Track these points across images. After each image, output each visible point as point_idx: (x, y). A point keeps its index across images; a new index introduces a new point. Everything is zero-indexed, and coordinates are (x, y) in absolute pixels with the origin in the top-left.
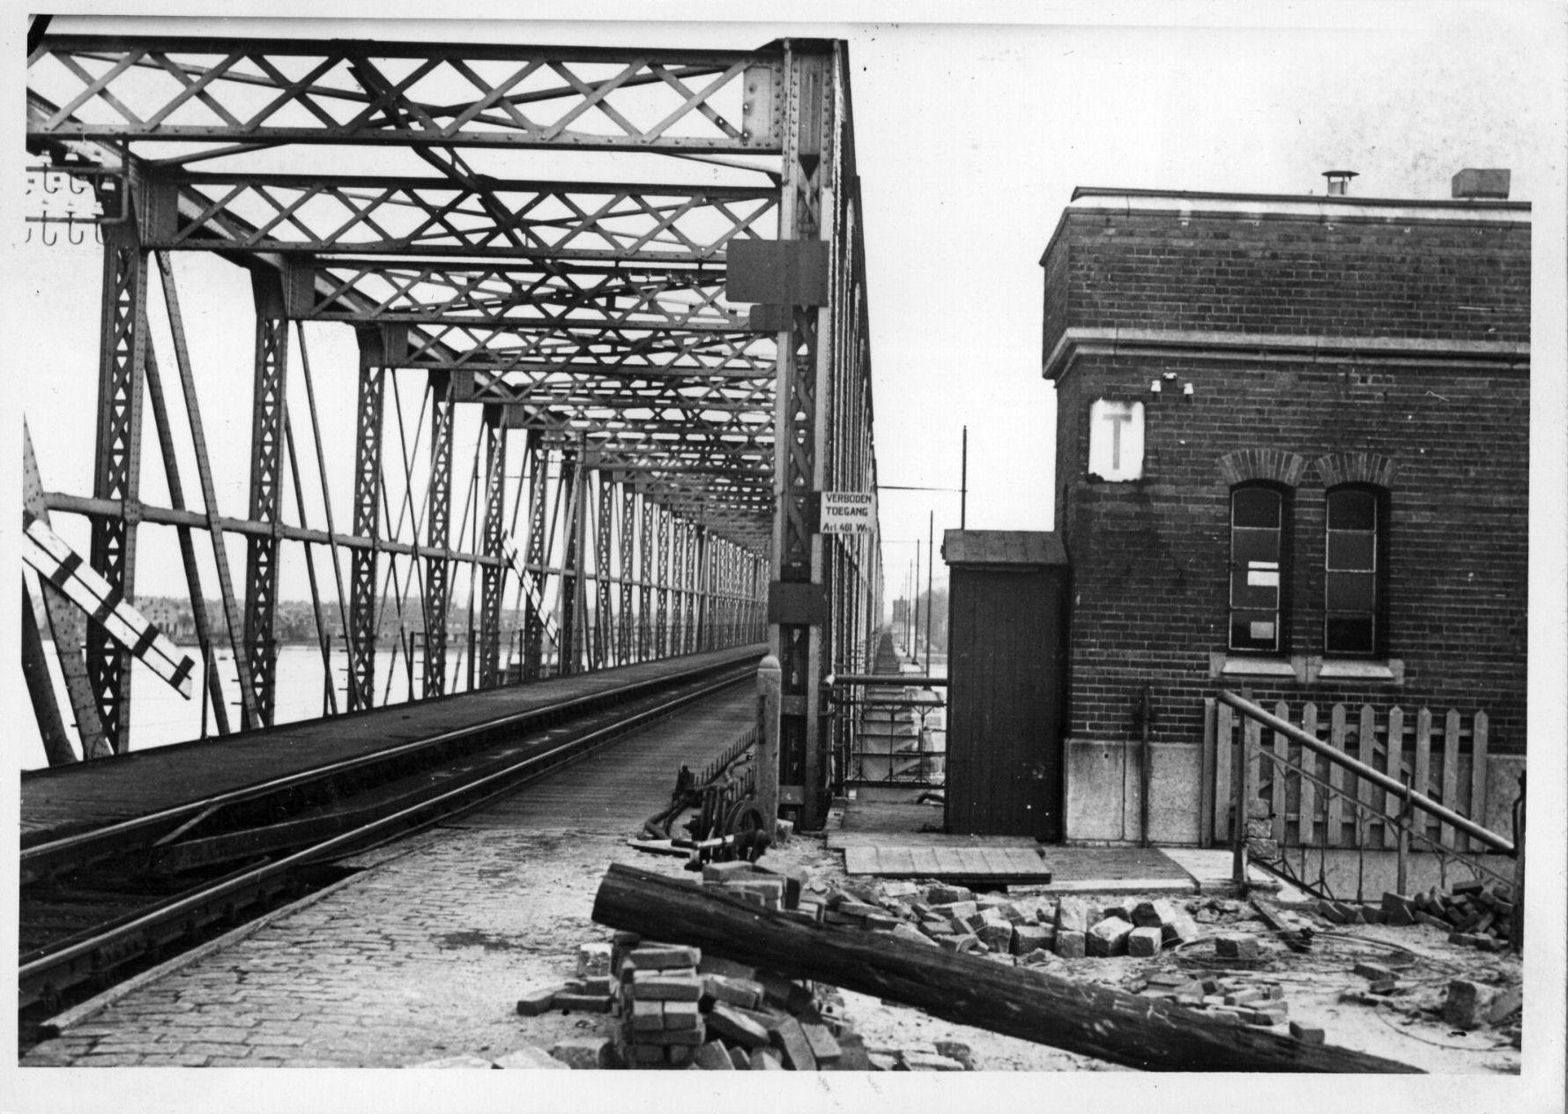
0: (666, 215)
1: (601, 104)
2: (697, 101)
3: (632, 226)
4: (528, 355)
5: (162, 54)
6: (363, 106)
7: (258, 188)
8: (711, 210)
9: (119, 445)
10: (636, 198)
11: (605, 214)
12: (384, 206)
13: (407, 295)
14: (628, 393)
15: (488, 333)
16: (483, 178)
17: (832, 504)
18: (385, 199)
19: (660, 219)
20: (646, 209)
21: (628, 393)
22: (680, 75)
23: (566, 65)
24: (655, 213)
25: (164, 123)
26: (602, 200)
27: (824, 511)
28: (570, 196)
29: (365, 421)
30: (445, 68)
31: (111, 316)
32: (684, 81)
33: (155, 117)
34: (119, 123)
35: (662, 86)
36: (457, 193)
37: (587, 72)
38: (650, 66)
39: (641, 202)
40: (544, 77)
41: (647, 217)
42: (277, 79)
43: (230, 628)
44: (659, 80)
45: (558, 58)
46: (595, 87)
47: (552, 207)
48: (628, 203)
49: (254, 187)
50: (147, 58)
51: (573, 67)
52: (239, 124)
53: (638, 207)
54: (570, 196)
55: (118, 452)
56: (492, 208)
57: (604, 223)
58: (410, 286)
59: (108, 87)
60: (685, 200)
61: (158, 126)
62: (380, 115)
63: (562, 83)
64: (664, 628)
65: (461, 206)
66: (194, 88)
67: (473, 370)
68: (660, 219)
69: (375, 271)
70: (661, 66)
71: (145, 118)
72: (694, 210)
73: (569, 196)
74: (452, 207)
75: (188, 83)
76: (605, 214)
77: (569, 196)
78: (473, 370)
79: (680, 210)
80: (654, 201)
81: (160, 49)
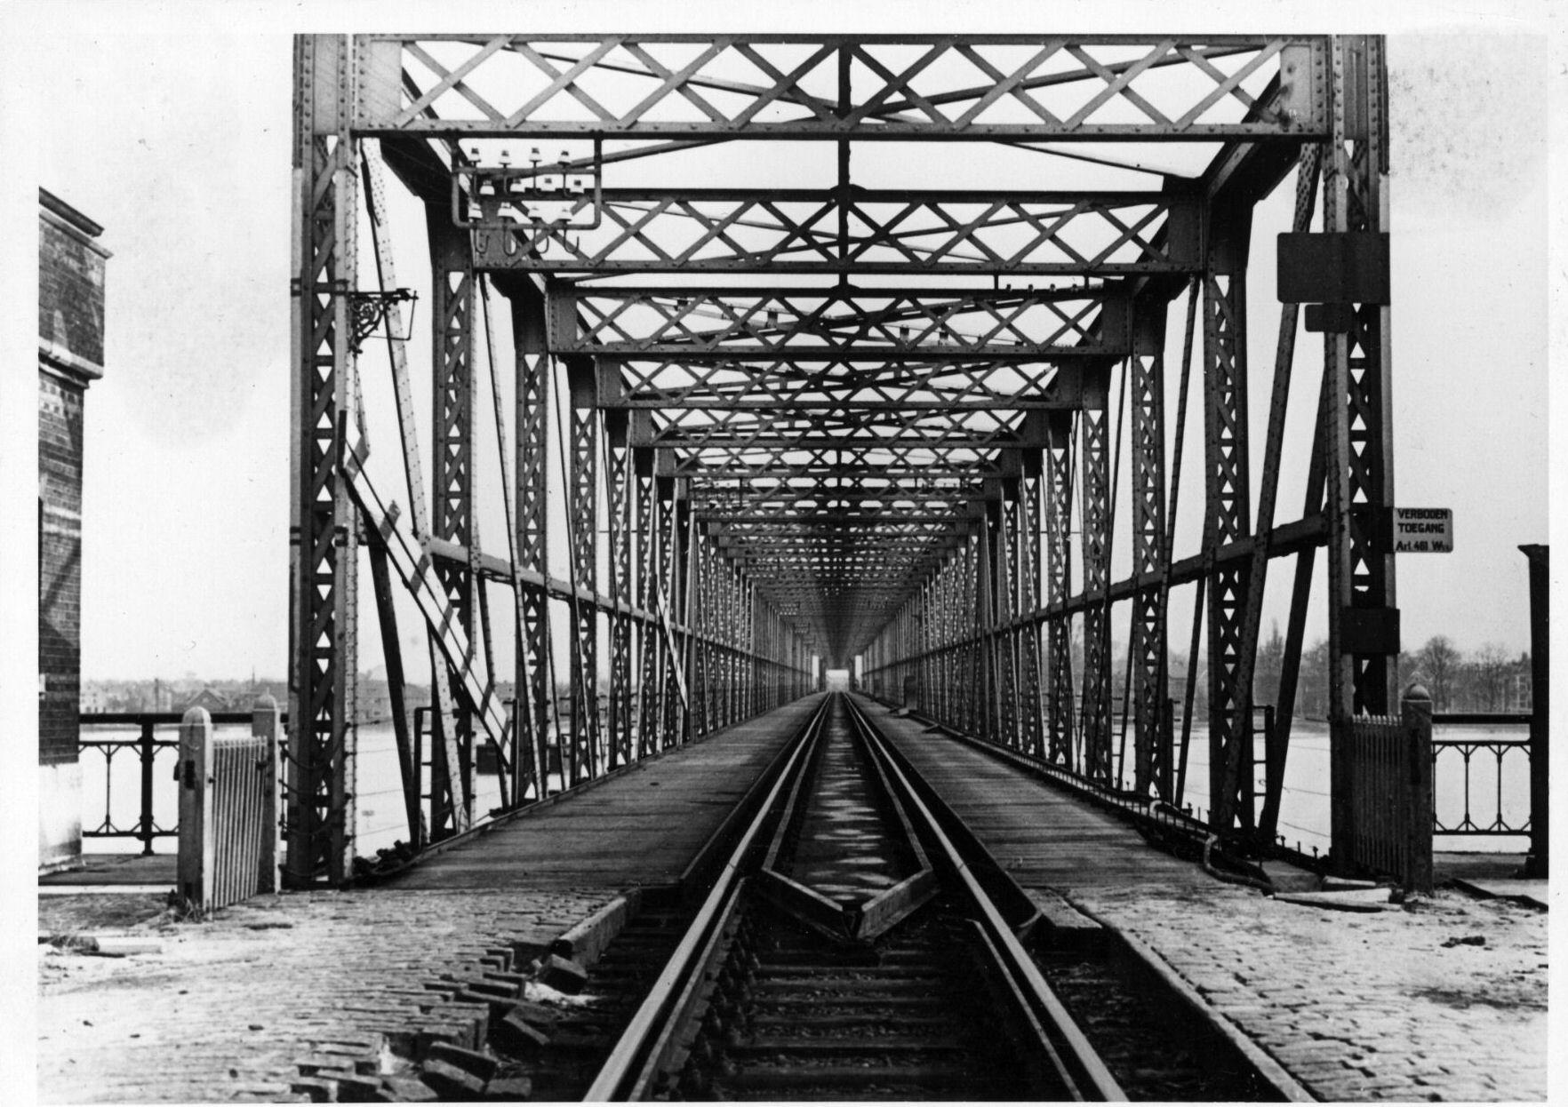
0: (1047, 223)
1: (1125, 91)
2: (1231, 85)
3: (1007, 239)
4: (751, 392)
8: (1095, 218)
9: (455, 487)
10: (1014, 206)
11: (983, 222)
12: (661, 216)
13: (678, 325)
14: (819, 434)
17: (1404, 521)
18: (662, 210)
19: (1041, 228)
20: (1023, 217)
21: (819, 434)
22: (1207, 57)
24: (1034, 220)
25: (642, 119)
26: (980, 209)
27: (1396, 529)
28: (942, 206)
29: (589, 467)
30: (952, 54)
31: (441, 346)
32: (1211, 61)
33: (631, 113)
34: (590, 119)
35: (1187, 68)
37: (1105, 55)
38: (1177, 47)
41: (1025, 225)
42: (655, 71)
43: (316, 683)
44: (1185, 60)
46: (1120, 69)
47: (923, 217)
48: (1006, 212)
52: (1058, 121)
54: (942, 206)
55: (455, 495)
57: (979, 233)
59: (576, 82)
60: (1069, 207)
61: (748, 122)
63: (1078, 66)
64: (628, 697)
65: (743, 218)
67: (650, 409)
68: (1041, 228)
70: (1188, 47)
71: (1174, 119)
72: (1080, 218)
73: (775, 204)
74: (734, 218)
75: (555, 75)
76: (983, 222)
77: (775, 204)
78: (650, 409)
79: (1064, 218)
80: (1032, 209)
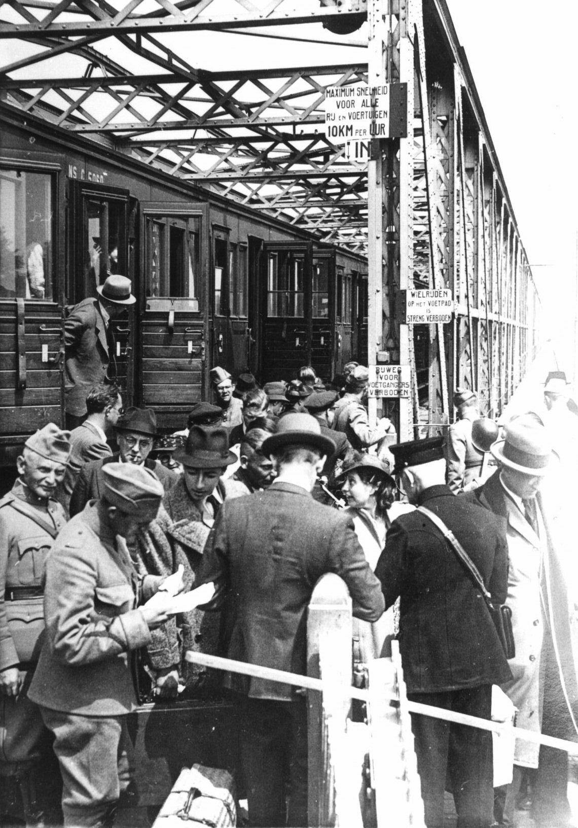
5: (107, 87)
6: (211, 105)
7: (57, 89)
15: (257, 185)
16: (200, 72)
23: (312, 77)
26: (281, 82)
30: (249, 84)
36: (183, 85)
38: (356, 73)
39: (312, 83)
40: (301, 85)
45: (307, 74)
49: (54, 88)
50: (100, 89)
51: (316, 78)
53: (311, 88)
56: (215, 95)
58: (190, 156)
62: (221, 109)
66: (125, 104)
69: (168, 147)
77: (262, 81)
81: (105, 84)
